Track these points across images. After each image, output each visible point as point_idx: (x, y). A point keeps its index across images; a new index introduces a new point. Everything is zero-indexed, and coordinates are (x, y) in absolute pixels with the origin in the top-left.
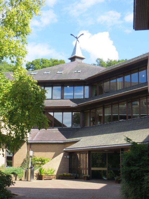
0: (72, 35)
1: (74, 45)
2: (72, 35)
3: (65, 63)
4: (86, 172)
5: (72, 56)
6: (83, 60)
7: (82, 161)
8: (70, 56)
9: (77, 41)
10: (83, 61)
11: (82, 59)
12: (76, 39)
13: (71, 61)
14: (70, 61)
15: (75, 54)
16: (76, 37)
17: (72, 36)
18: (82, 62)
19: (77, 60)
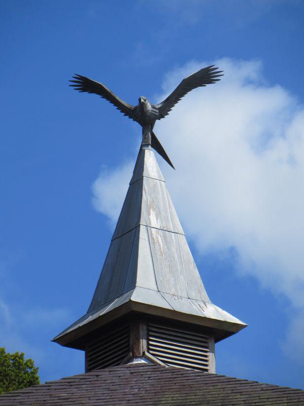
0: (87, 85)
1: (115, 214)
2: (87, 85)
3: (32, 382)
4: (120, 340)
5: (95, 305)
6: (219, 345)
7: (118, 342)
8: (72, 313)
9: (150, 156)
10: (214, 362)
11: (208, 333)
12: (137, 127)
13: (92, 364)
14: (76, 360)
15: (133, 285)
16: (130, 102)
17: (96, 97)
18: (212, 369)
19: (152, 353)
